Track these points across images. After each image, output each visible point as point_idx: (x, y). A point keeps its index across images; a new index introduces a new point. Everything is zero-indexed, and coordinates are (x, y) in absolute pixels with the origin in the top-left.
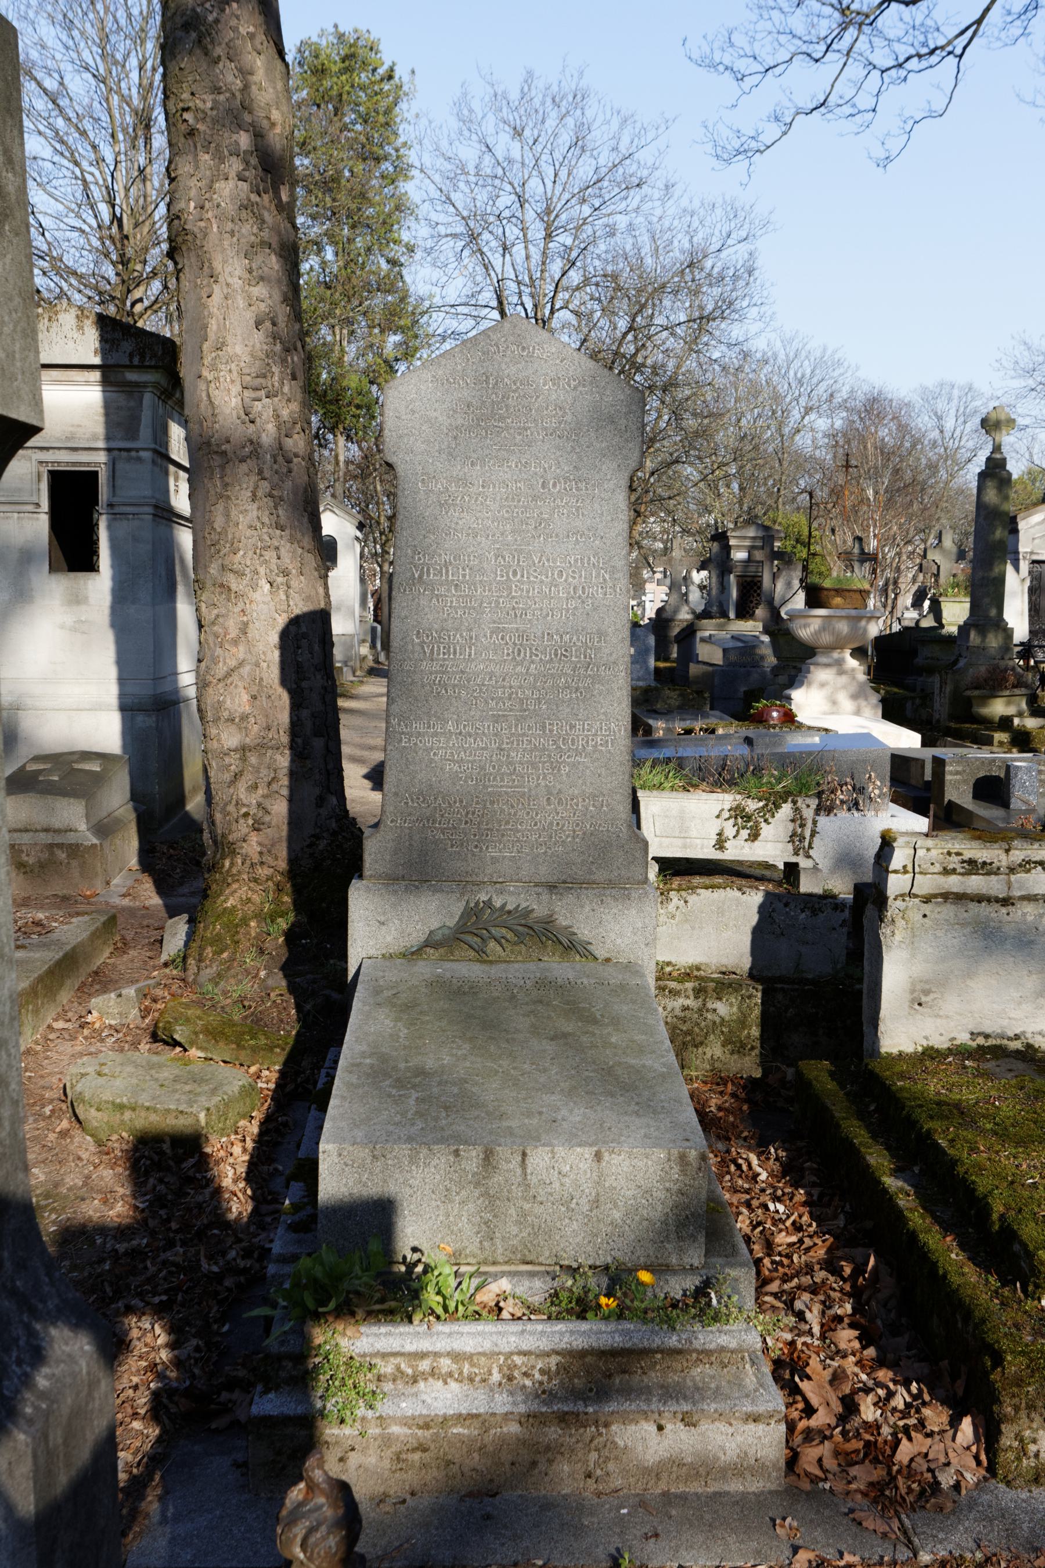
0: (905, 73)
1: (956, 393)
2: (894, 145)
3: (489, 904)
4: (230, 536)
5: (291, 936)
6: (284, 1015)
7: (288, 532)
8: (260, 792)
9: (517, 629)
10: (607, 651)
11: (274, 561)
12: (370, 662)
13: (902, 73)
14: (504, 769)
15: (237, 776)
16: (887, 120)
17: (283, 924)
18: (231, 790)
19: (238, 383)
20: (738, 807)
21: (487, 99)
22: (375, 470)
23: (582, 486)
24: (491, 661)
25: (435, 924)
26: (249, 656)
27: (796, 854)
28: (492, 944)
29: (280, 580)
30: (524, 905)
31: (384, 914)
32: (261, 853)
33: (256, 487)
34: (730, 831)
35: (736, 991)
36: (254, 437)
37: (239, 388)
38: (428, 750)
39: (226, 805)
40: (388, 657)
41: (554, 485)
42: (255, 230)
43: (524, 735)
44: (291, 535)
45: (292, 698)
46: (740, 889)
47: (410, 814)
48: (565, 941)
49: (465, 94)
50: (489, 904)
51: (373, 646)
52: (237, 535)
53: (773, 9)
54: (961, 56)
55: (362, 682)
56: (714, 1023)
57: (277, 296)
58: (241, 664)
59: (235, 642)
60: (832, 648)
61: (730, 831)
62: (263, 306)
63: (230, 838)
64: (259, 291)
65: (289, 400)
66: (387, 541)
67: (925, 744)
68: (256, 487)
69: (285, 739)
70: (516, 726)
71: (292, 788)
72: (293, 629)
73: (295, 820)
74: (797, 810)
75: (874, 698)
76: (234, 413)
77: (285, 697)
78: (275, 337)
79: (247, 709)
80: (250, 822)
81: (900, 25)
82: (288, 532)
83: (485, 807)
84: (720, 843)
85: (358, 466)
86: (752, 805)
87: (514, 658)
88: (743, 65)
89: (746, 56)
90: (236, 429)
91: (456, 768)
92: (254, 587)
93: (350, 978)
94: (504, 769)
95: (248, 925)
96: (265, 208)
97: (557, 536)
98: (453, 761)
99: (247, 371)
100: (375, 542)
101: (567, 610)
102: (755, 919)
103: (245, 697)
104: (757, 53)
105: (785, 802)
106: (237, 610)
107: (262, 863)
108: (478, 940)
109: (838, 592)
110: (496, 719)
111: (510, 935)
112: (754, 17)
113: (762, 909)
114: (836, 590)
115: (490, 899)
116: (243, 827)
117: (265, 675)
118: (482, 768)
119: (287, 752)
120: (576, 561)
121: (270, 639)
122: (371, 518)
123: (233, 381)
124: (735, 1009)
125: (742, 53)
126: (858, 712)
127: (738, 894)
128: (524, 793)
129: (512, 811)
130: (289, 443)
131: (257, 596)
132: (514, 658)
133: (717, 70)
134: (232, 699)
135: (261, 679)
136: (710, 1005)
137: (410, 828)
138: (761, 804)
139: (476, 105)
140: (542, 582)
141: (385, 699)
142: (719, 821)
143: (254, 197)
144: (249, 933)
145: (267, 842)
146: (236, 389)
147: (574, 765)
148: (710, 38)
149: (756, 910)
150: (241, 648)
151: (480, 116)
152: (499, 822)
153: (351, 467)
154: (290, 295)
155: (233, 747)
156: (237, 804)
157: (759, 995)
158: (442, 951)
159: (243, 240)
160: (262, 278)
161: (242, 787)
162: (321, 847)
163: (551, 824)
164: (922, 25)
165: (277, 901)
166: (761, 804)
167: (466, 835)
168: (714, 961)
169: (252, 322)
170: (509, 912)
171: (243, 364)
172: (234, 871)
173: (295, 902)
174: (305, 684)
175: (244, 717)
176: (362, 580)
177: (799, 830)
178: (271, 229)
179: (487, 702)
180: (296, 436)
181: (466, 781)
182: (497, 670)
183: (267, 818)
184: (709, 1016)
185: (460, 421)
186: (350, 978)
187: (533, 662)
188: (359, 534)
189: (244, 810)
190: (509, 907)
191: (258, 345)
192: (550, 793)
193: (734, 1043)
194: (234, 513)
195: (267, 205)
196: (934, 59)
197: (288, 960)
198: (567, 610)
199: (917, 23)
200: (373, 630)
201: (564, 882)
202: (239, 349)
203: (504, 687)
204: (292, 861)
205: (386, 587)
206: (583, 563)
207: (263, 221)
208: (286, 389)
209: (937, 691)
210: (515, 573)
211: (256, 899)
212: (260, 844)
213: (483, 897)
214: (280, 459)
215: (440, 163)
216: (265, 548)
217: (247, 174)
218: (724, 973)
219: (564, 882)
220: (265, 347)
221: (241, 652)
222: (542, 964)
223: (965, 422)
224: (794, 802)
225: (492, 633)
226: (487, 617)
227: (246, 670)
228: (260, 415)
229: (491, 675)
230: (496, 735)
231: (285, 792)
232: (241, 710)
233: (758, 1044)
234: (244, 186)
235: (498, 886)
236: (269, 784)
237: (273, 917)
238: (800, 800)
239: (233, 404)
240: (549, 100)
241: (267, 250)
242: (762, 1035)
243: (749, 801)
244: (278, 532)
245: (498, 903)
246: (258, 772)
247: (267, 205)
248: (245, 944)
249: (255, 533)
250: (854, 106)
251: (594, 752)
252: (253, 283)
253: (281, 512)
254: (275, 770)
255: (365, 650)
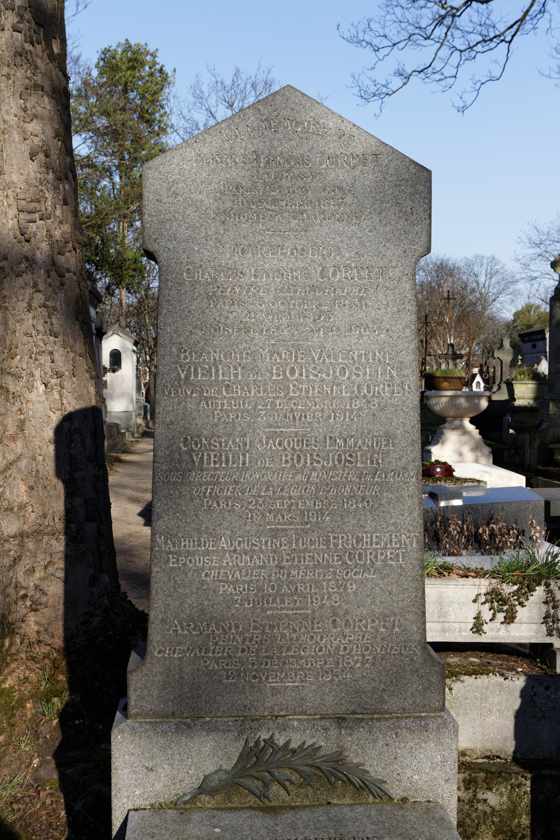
0: (474, 53)
1: (485, 261)
2: (469, 98)
3: (270, 742)
4: (8, 343)
5: (65, 716)
6: (53, 820)
7: (61, 338)
8: (37, 575)
9: (296, 434)
10: (395, 455)
11: (49, 364)
12: (143, 428)
13: (473, 54)
14: (285, 589)
15: (16, 561)
16: (464, 82)
17: (58, 703)
18: (11, 574)
19: (15, 207)
20: (493, 591)
21: (211, 85)
22: (145, 310)
23: (365, 273)
24: (267, 469)
25: (210, 768)
26: (25, 451)
27: (550, 634)
28: (275, 788)
29: (54, 381)
30: (309, 742)
31: (152, 758)
32: (38, 632)
33: (32, 299)
34: (487, 615)
35: (506, 780)
36: (29, 254)
37: (15, 211)
38: (198, 571)
39: (6, 587)
40: (154, 423)
41: (334, 274)
42: (29, 74)
43: (305, 550)
44: (64, 341)
45: (66, 488)
46: (502, 675)
47: (180, 644)
48: (356, 781)
49: (198, 82)
50: (270, 742)
51: (145, 418)
52: (14, 342)
53: (396, 6)
54: (510, 42)
55: (138, 441)
56: (485, 813)
57: (50, 132)
58: (19, 458)
59: (13, 438)
60: (455, 417)
61: (487, 615)
62: (36, 140)
63: (10, 619)
64: (34, 127)
65: (61, 222)
66: (153, 353)
67: (528, 484)
68: (32, 299)
69: (60, 526)
70: (297, 541)
71: (68, 570)
72: (66, 425)
73: (70, 599)
74: (549, 592)
75: (487, 450)
76: (11, 234)
77: (60, 486)
78: (48, 167)
79: (25, 499)
80: (28, 603)
81: (470, 25)
82: (61, 338)
83: (263, 633)
84: (478, 627)
85: (135, 308)
86: (508, 589)
87: (293, 466)
88: (377, 42)
89: (380, 36)
90: (13, 248)
91: (230, 590)
92: (31, 388)
93: (114, 833)
94: (285, 589)
95: (24, 707)
96: (38, 56)
97: (338, 329)
98: (227, 582)
99: (23, 196)
100: (146, 354)
101: (351, 411)
102: (517, 703)
103: (23, 488)
104: (387, 34)
105: (539, 584)
106: (15, 409)
107: (39, 642)
108: (259, 784)
109: (446, 379)
110: (275, 534)
111: (295, 777)
112: (383, 13)
113: (524, 693)
114: (444, 378)
115: (272, 737)
116: (22, 609)
117: (40, 468)
118: (260, 589)
119: (62, 537)
120: (360, 356)
121: (45, 435)
122: (143, 339)
123: (9, 206)
124: (505, 798)
125: (378, 34)
126: (477, 461)
127: (501, 679)
128: (307, 615)
129: (294, 636)
130: (61, 259)
131: (32, 396)
132: (293, 466)
133: (361, 45)
134: (11, 491)
135: (38, 471)
136: (480, 796)
137: (180, 659)
138: (516, 587)
139: (205, 89)
140: (322, 380)
141: (152, 453)
142: (476, 605)
143: (28, 46)
144: (25, 715)
145: (44, 621)
146: (12, 212)
147: (362, 583)
148: (355, 24)
149: (518, 694)
150: (19, 444)
151: (207, 94)
152: (280, 648)
153: (131, 309)
154: (62, 131)
155: (13, 534)
156: (16, 586)
157: (528, 783)
158: (218, 797)
159: (17, 83)
160: (35, 116)
161: (20, 570)
162: (94, 624)
163: (338, 648)
164: (485, 23)
165: (51, 679)
166: (516, 587)
167: (243, 664)
168: (479, 746)
169: (27, 154)
170: (294, 751)
171: (18, 190)
172: (13, 650)
173: (70, 681)
174: (78, 475)
175: (22, 507)
176: (138, 377)
177: (552, 611)
178: (44, 75)
179: (264, 516)
180: (68, 254)
181: (242, 604)
182: (275, 479)
183: (44, 599)
184: (480, 807)
185: (229, 204)
186: (114, 833)
187: (314, 469)
188: (135, 348)
189: (22, 592)
190: (294, 745)
191: (32, 174)
192: (335, 614)
193: (505, 832)
194: (11, 322)
195: (40, 54)
196: (493, 45)
197: (61, 744)
198: (351, 411)
199: (482, 23)
200: (145, 407)
201: (354, 713)
202: (15, 177)
203: (282, 498)
204: (68, 638)
205: (153, 380)
206: (367, 359)
207: (36, 68)
208: (58, 213)
209: (527, 445)
210: (292, 371)
211: (33, 677)
212: (37, 623)
213: (264, 735)
214: (53, 274)
215: (182, 123)
216: (41, 353)
217: (21, 26)
218: (488, 757)
219: (354, 713)
220: (39, 176)
221: (18, 447)
222: (333, 811)
223: (491, 278)
224: (547, 585)
225: (268, 438)
226: (262, 420)
227: (23, 463)
228: (35, 235)
229: (268, 485)
230: (275, 551)
231: (61, 574)
232: (19, 500)
233: (528, 832)
234: (19, 36)
235: (280, 720)
236: (46, 567)
237: (47, 698)
238: (552, 583)
239: (10, 226)
240: (249, 86)
241: (40, 93)
242: (532, 824)
243: (504, 586)
244: (52, 338)
245: (281, 741)
246: (35, 556)
247: (40, 54)
248: (21, 727)
249: (31, 340)
250: (442, 74)
251: (384, 567)
252: (28, 120)
253: (54, 321)
254: (51, 555)
255: (140, 421)
